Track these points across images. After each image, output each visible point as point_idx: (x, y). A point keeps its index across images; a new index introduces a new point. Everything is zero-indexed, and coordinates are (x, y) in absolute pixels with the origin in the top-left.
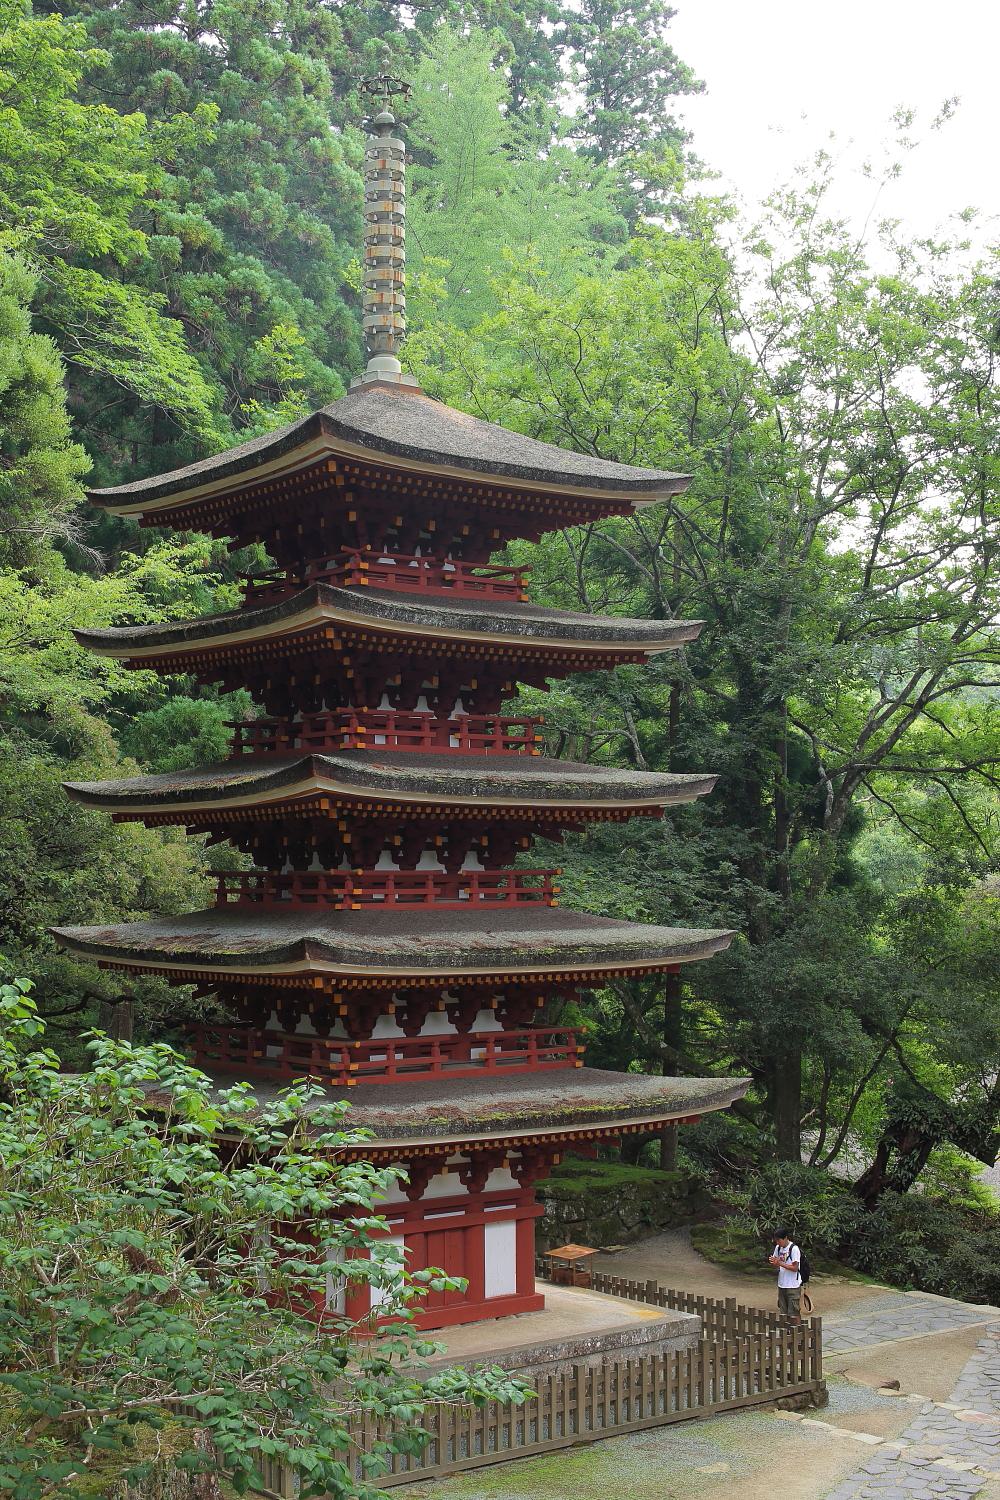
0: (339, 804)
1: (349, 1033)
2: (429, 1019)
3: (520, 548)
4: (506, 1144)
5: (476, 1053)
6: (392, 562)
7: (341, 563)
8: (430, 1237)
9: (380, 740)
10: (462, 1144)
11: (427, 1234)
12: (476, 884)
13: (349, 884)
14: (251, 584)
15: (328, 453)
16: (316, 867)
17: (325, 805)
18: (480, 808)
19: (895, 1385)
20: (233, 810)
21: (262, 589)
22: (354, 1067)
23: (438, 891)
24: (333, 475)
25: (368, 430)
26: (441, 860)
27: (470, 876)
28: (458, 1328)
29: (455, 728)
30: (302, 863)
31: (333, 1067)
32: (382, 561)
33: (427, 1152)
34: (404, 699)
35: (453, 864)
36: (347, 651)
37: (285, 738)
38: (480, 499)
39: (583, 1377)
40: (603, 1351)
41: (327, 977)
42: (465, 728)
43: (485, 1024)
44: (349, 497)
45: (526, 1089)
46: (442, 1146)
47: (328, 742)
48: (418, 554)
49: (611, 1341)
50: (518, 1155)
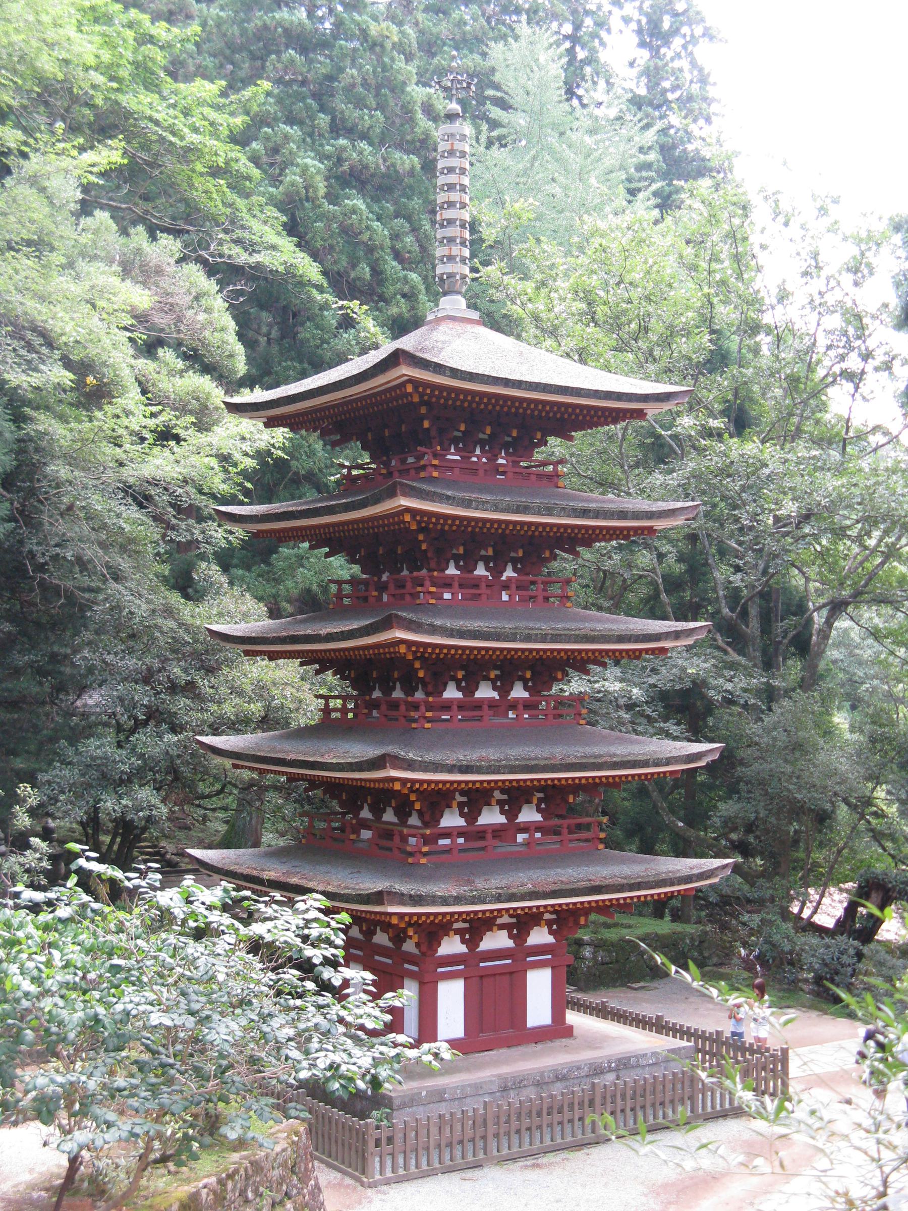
0: (414, 649)
1: (423, 822)
2: (485, 811)
3: (555, 446)
4: (542, 910)
5: (520, 838)
6: (458, 458)
7: (419, 457)
8: (485, 980)
9: (447, 596)
10: (507, 910)
11: (481, 977)
12: (521, 707)
13: (423, 708)
14: (349, 472)
15: (406, 378)
16: (398, 694)
17: (403, 649)
18: (523, 650)
19: (849, 1102)
20: (335, 650)
21: (358, 477)
22: (425, 849)
23: (491, 712)
24: (410, 394)
25: (435, 360)
26: (495, 688)
27: (517, 700)
28: (503, 1051)
29: (506, 586)
30: (388, 691)
31: (409, 849)
32: (449, 457)
33: (480, 915)
34: (467, 563)
35: (504, 691)
36: (421, 530)
37: (375, 593)
38: (525, 410)
39: (599, 1091)
40: (617, 1070)
41: (404, 781)
42: (514, 586)
43: (529, 815)
44: (423, 410)
45: (557, 867)
46: (492, 911)
47: (408, 598)
48: (478, 452)
49: (624, 1063)
50: (554, 916)
